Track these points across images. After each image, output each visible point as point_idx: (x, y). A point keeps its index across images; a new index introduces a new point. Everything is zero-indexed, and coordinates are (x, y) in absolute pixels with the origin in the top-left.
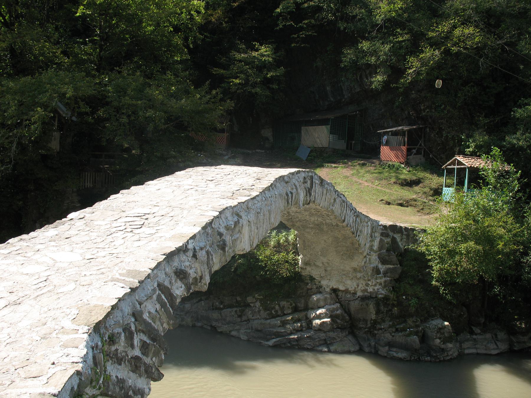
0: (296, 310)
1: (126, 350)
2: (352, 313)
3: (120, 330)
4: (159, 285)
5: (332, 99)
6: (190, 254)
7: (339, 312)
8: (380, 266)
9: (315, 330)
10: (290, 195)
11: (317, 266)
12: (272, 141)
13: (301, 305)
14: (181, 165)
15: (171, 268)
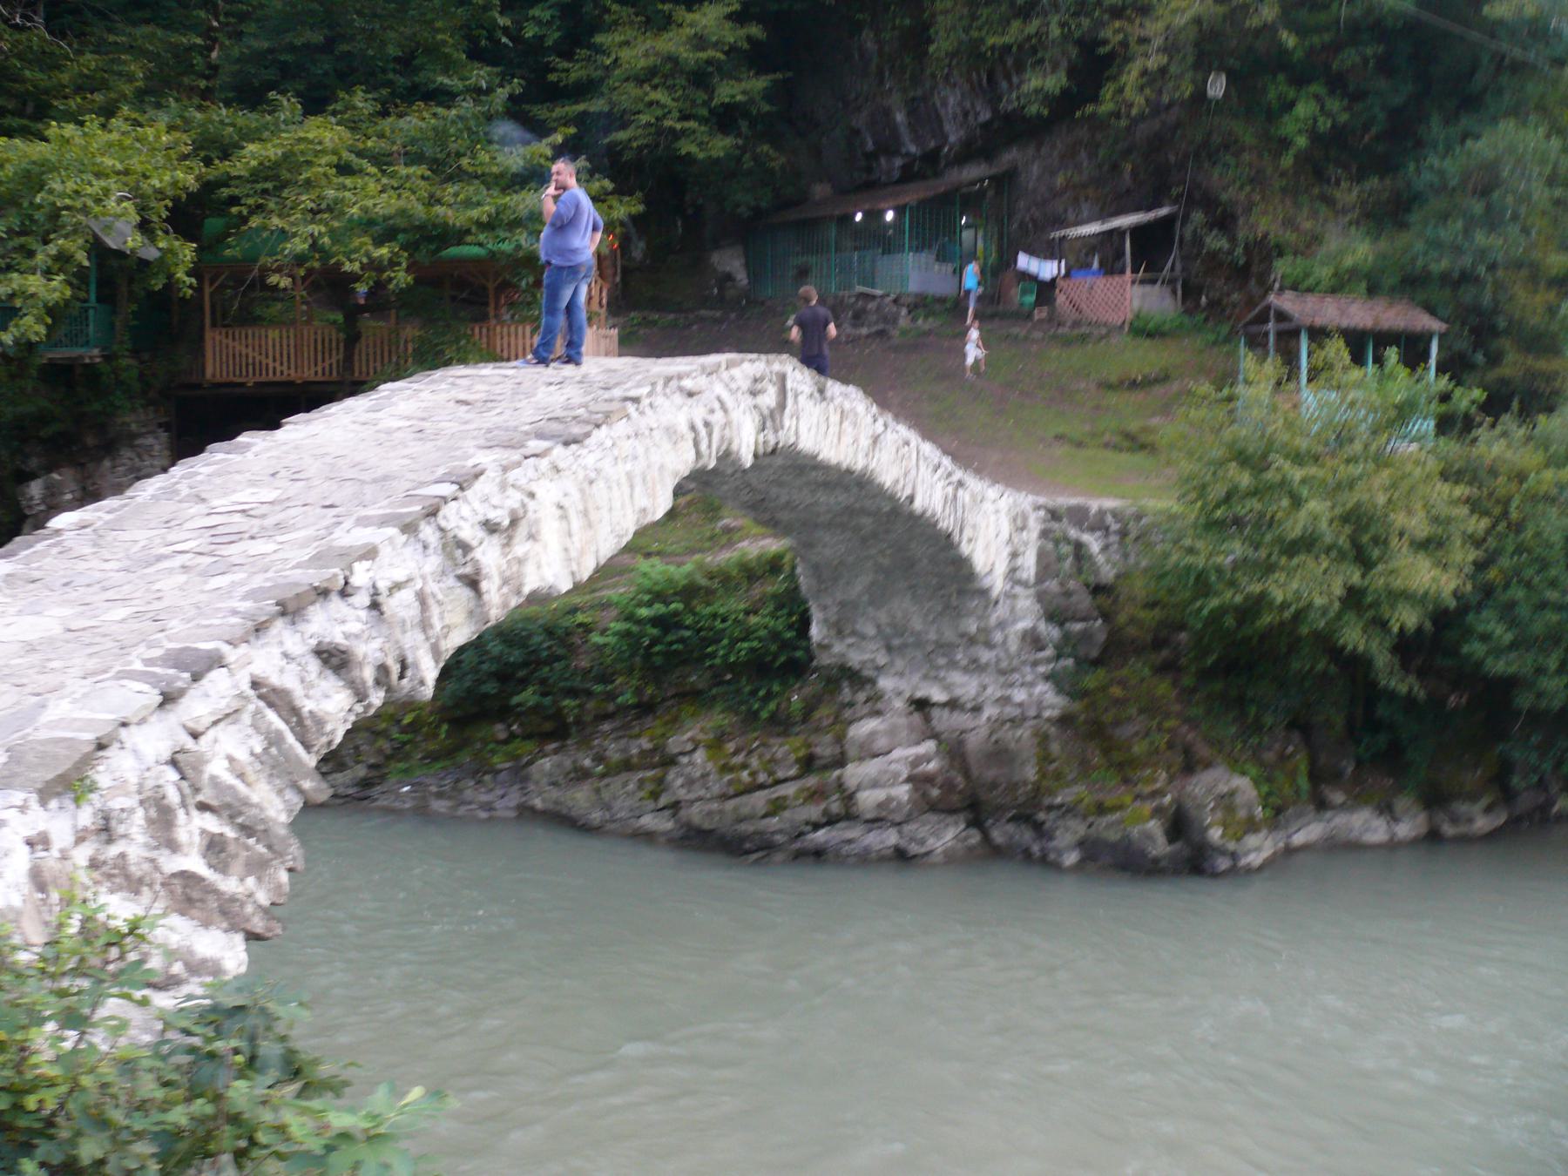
0: (808, 764)
1: (154, 854)
2: (972, 761)
3: (130, 802)
4: (255, 685)
5: (913, 149)
6: (362, 599)
7: (932, 766)
8: (1043, 627)
9: (867, 821)
10: (703, 432)
11: (863, 637)
12: (745, 282)
13: (825, 748)
14: (389, 369)
15: (303, 640)
